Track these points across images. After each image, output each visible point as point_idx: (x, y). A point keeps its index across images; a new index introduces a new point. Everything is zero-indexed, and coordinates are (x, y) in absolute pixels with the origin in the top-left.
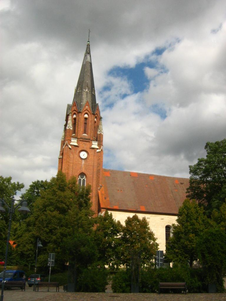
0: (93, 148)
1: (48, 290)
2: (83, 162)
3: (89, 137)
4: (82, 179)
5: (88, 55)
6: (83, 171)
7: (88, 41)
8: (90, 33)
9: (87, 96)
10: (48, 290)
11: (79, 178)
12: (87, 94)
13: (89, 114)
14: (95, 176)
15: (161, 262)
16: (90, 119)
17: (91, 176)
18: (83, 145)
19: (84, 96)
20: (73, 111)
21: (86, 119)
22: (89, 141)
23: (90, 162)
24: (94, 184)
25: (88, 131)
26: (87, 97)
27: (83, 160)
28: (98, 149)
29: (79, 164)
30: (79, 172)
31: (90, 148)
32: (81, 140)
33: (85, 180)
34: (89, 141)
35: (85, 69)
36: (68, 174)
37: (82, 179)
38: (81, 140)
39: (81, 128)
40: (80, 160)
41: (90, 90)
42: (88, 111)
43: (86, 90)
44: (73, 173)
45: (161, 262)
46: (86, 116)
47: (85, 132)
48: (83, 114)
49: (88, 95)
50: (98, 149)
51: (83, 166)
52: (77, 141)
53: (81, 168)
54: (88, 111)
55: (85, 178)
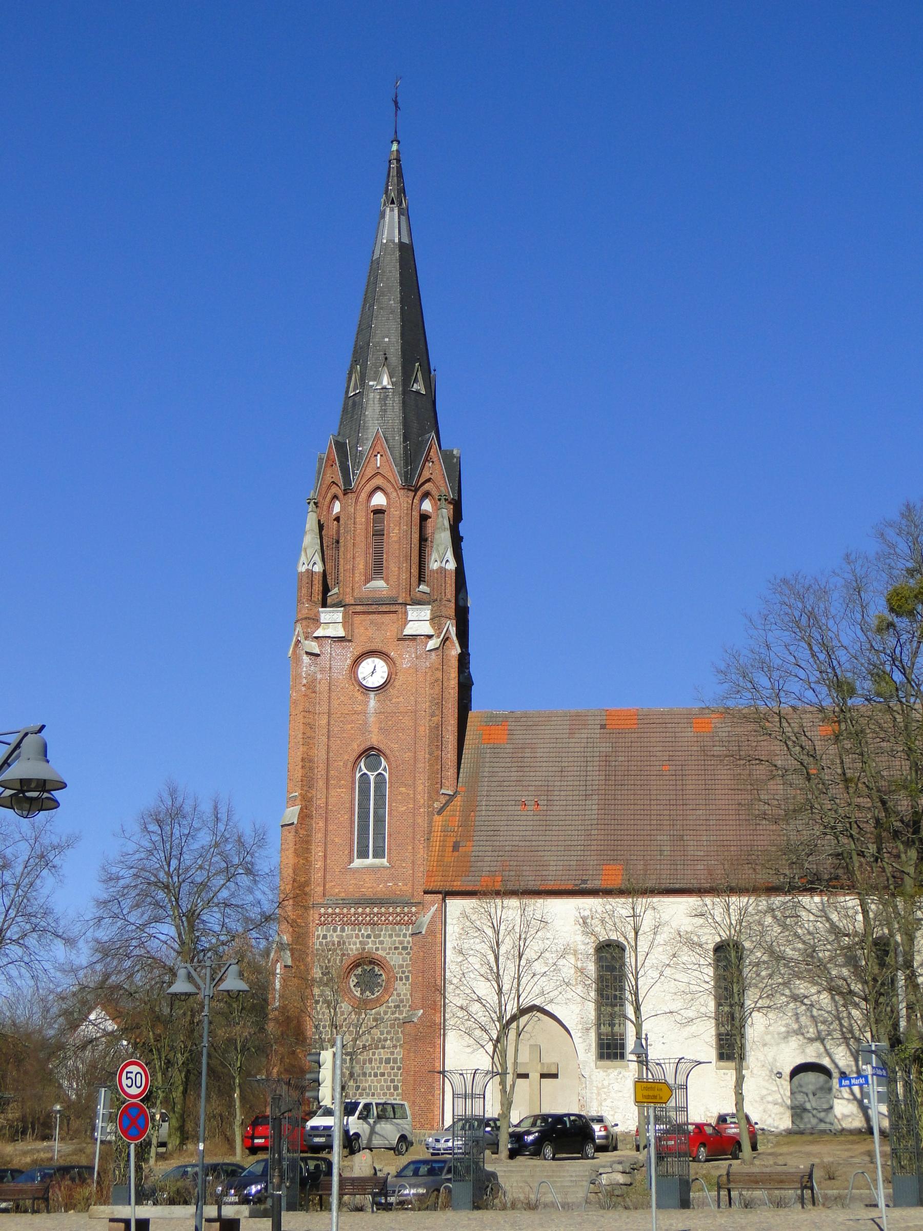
0: (413, 637)
1: (440, 1072)
2: (372, 702)
3: (394, 593)
4: (372, 776)
5: (392, 210)
6: (374, 739)
7: (393, 137)
8: (399, 112)
9: (385, 411)
10: (440, 1072)
11: (361, 770)
12: (383, 400)
13: (390, 489)
14: (423, 754)
15: (880, 1089)
16: (394, 513)
17: (408, 755)
18: (369, 631)
19: (372, 410)
20: (329, 487)
21: (378, 511)
22: (393, 608)
23: (401, 699)
24: (420, 788)
25: (388, 568)
26: (384, 411)
27: (372, 695)
28: (430, 637)
29: (356, 713)
30: (356, 747)
31: (399, 640)
32: (359, 608)
33: (387, 775)
34: (393, 608)
35: (375, 283)
36: (310, 761)
37: (372, 776)
38: (359, 608)
39: (356, 557)
40: (357, 694)
41: (398, 378)
42: (384, 477)
43: (380, 382)
44: (331, 754)
45: (880, 1089)
46: (379, 500)
47: (377, 569)
48: (363, 495)
49: (389, 402)
50: (430, 637)
51: (372, 719)
52: (344, 617)
53: (364, 729)
54: (384, 477)
55: (385, 769)
